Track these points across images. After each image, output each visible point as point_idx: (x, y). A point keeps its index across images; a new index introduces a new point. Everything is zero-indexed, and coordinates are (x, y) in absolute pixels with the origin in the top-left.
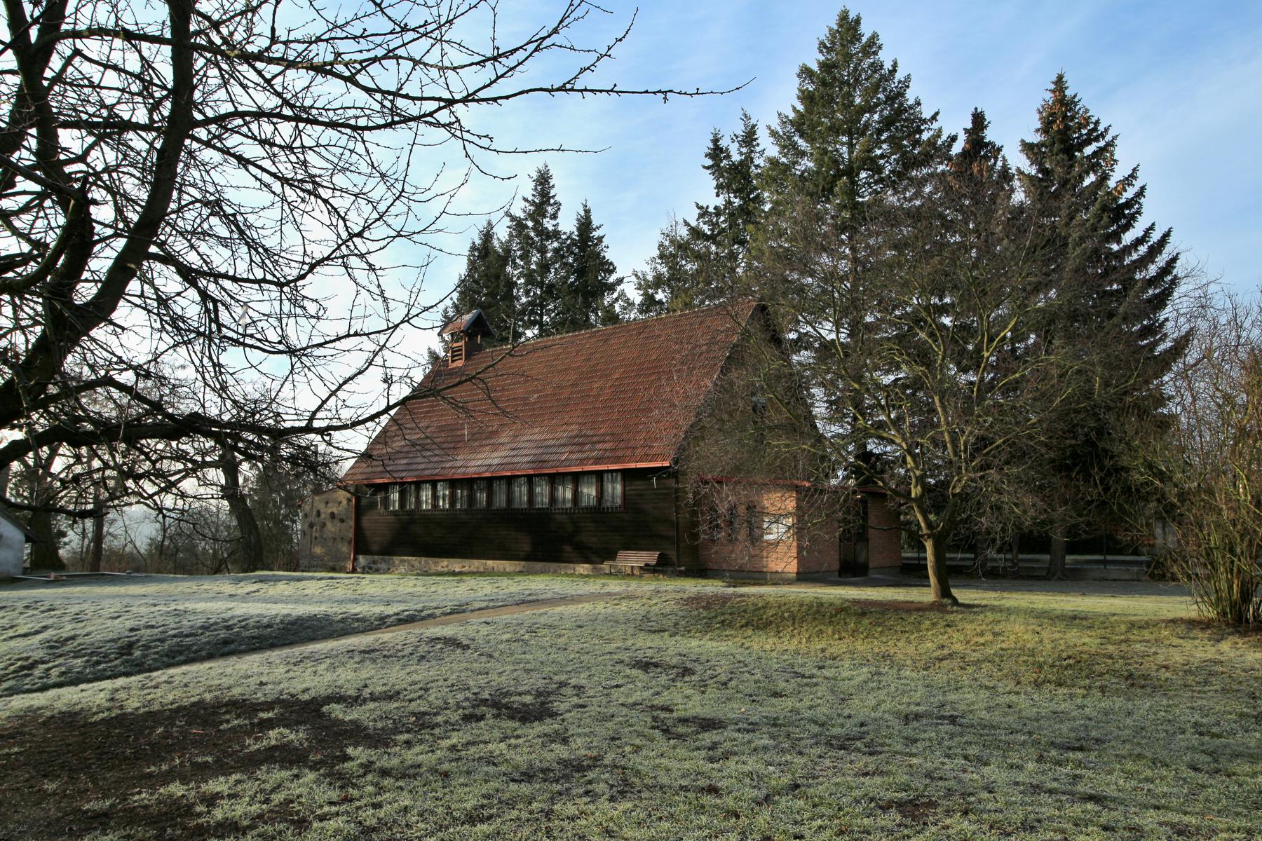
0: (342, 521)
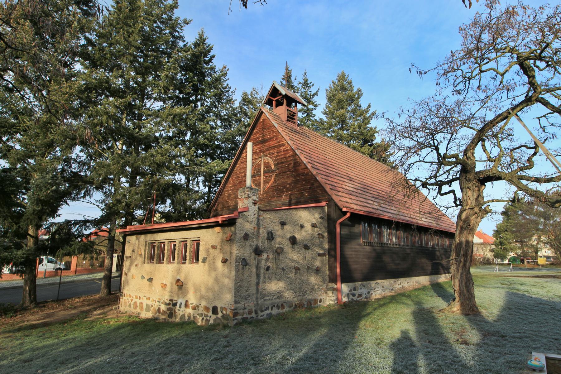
0: (306, 247)
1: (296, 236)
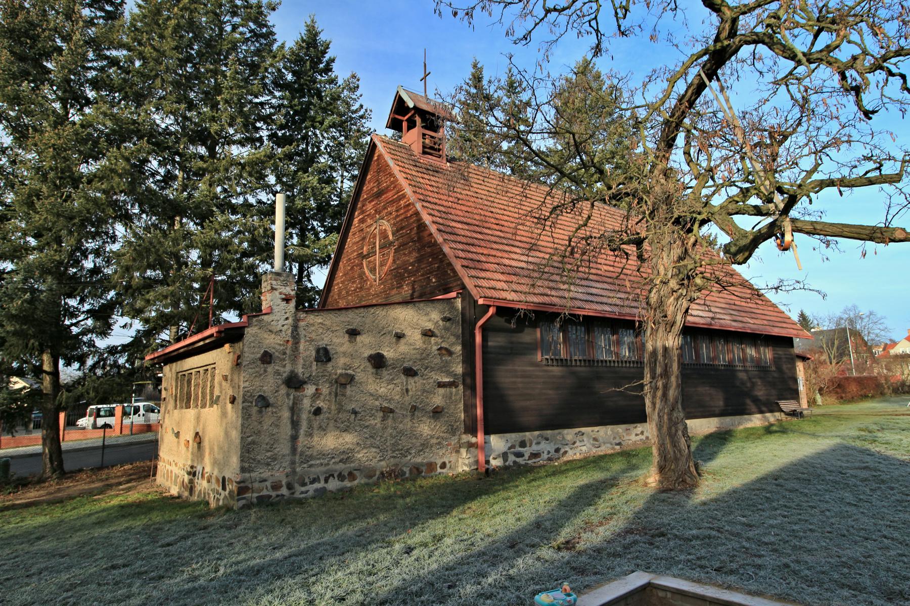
0: (410, 372)
1: (385, 354)
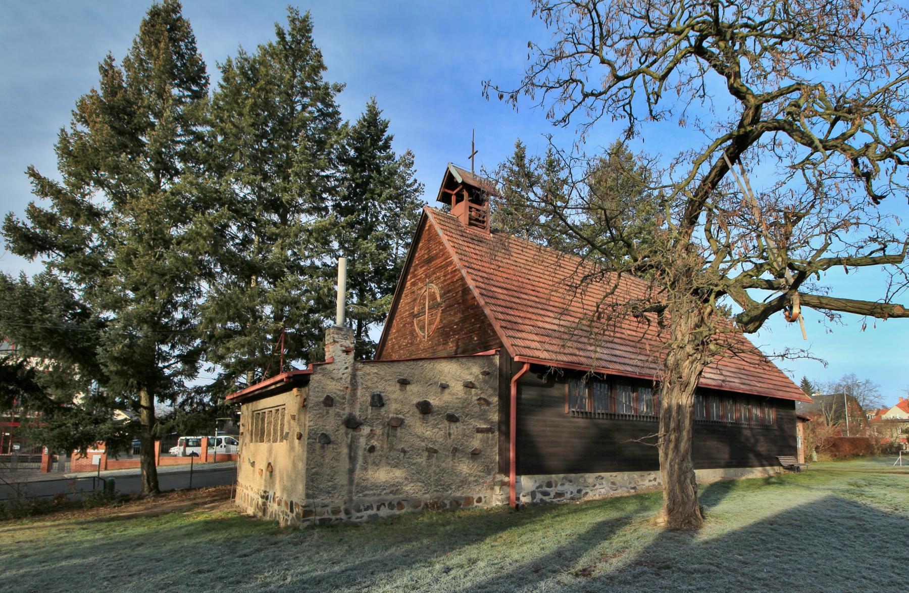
0: (452, 419)
1: (431, 402)
